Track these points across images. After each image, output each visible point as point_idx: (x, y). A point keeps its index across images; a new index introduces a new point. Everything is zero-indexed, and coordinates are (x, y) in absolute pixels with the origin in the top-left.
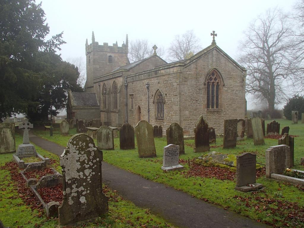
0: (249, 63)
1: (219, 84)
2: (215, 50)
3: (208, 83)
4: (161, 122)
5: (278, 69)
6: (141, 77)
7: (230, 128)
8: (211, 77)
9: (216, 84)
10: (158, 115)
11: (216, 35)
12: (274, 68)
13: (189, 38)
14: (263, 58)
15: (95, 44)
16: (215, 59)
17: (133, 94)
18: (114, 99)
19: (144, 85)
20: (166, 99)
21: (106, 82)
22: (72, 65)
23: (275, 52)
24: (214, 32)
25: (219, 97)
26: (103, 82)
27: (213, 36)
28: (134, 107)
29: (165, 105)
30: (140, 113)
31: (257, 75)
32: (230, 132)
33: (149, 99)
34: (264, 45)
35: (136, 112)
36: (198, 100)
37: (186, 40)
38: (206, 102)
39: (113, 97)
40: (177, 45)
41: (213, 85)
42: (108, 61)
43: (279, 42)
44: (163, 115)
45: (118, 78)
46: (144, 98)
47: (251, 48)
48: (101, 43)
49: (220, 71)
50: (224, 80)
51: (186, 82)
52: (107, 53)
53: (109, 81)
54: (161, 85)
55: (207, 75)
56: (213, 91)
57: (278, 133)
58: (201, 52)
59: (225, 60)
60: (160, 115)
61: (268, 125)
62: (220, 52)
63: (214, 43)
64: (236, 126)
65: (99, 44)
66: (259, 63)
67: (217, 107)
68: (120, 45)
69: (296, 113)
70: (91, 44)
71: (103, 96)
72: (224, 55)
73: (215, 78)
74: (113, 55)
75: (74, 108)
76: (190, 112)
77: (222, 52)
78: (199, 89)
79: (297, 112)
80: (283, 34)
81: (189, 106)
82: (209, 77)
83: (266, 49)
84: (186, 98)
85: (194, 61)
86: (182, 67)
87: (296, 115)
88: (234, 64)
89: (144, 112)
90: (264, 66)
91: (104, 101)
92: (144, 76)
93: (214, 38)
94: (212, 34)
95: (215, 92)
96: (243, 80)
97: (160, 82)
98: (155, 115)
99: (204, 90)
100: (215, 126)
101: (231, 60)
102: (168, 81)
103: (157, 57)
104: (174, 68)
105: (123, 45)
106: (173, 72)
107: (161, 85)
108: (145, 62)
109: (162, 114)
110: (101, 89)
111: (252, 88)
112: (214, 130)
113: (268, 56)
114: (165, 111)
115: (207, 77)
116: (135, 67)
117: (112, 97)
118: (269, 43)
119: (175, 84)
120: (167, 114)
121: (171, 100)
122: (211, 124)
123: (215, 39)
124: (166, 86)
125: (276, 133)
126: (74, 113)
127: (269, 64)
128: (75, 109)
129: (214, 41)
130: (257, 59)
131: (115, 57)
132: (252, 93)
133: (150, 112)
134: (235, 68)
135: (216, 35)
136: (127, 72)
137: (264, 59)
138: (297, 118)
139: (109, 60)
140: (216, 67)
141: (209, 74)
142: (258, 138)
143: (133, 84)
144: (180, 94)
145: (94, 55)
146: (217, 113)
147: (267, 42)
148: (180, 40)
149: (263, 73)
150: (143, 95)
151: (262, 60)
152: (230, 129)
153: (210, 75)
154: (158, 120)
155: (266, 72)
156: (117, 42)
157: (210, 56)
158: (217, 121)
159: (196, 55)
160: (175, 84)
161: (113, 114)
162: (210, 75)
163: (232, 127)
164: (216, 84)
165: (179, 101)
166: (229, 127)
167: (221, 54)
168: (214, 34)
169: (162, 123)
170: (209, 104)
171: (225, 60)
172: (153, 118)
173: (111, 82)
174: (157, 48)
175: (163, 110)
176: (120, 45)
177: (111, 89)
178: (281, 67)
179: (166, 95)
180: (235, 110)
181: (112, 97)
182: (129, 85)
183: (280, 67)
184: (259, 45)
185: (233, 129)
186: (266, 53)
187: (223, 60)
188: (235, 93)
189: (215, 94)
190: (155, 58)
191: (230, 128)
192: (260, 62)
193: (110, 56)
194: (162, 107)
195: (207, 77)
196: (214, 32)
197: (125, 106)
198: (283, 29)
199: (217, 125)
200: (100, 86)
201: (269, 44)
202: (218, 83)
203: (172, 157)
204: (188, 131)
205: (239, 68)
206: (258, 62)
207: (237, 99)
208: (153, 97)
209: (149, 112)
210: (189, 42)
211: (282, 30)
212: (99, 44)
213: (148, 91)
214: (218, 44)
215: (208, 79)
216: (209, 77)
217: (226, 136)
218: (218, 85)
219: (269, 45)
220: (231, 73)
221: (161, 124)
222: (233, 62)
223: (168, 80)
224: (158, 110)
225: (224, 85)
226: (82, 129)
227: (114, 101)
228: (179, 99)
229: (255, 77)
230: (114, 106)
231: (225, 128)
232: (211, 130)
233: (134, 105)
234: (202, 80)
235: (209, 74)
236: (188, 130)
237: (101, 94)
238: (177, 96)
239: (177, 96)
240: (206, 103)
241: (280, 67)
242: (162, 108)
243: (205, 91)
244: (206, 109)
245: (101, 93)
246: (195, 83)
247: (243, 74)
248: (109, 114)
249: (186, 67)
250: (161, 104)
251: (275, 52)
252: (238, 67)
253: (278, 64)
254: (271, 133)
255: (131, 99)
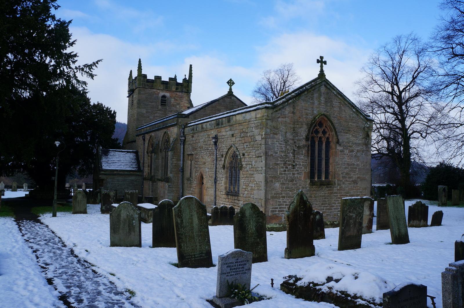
0: (373, 113)
1: (330, 140)
2: (323, 86)
3: (313, 138)
4: (235, 200)
5: (413, 123)
6: (206, 125)
7: (351, 214)
8: (317, 130)
9: (324, 140)
10: (230, 188)
11: (325, 63)
12: (407, 123)
13: (286, 76)
14: (392, 107)
15: (142, 77)
16: (324, 99)
17: (193, 153)
18: (164, 160)
19: (210, 139)
20: (243, 163)
21: (153, 134)
22: (99, 107)
23: (410, 98)
24: (322, 58)
25: (331, 161)
26: (149, 134)
27: (320, 63)
28: (193, 175)
29: (241, 172)
30: (203, 183)
31: (385, 132)
32: (351, 221)
33: (216, 162)
34: (393, 90)
35: (195, 183)
36: (296, 165)
37: (280, 78)
38: (308, 170)
39: (162, 158)
40: (265, 82)
41: (320, 142)
42: (160, 103)
43: (413, 85)
44: (238, 188)
45: (171, 128)
46: (209, 160)
47: (374, 92)
48: (151, 77)
49: (332, 119)
50: (338, 134)
51: (276, 134)
52: (159, 91)
53: (157, 132)
54: (237, 140)
55: (311, 125)
56: (321, 152)
57: (425, 222)
58: (302, 87)
59: (339, 102)
60: (234, 188)
61: (410, 207)
62: (331, 89)
63: (322, 74)
64: (361, 211)
65: (148, 78)
66: (388, 115)
67: (327, 177)
68: (180, 80)
69: (444, 189)
70: (136, 78)
71: (149, 156)
72: (338, 95)
73: (324, 130)
74: (168, 94)
75: (103, 172)
76: (283, 184)
77: (334, 90)
78: (299, 147)
79: (446, 187)
80: (419, 73)
81: (281, 174)
82: (314, 128)
83: (397, 94)
84: (277, 162)
85: (291, 101)
86: (271, 111)
87: (444, 192)
88: (354, 110)
89: (208, 182)
90: (394, 119)
91: (150, 164)
92: (210, 124)
93: (322, 67)
94: (318, 61)
95: (324, 152)
96: (368, 136)
97: (235, 135)
98: (226, 188)
99: (306, 148)
100: (324, 209)
101: (349, 103)
102: (247, 133)
103: (233, 98)
104: (257, 111)
105: (185, 80)
106: (256, 118)
107: (237, 140)
108: (214, 104)
109: (237, 187)
110: (146, 145)
111: (377, 150)
112: (321, 215)
113: (400, 104)
114: (242, 181)
115: (310, 128)
116: (198, 112)
117: (160, 158)
118: (400, 86)
119: (259, 138)
120: (244, 187)
121: (252, 165)
122: (316, 204)
123: (324, 69)
124: (243, 142)
125: (422, 221)
126: (103, 180)
127: (401, 116)
128: (105, 174)
129: (322, 71)
130: (384, 108)
131: (171, 97)
132: (376, 158)
133: (218, 182)
134: (355, 115)
135: (325, 63)
136: (185, 119)
137: (394, 108)
138: (445, 196)
139: (162, 102)
140: (326, 113)
141: (314, 122)
142: (400, 232)
143: (193, 137)
144: (266, 153)
145: (139, 93)
146: (327, 187)
147: (397, 84)
148: (271, 79)
149: (394, 128)
150: (208, 155)
151: (391, 110)
152: (351, 217)
153: (315, 126)
154: (230, 197)
155: (398, 128)
156: (176, 76)
157: (316, 95)
158: (327, 200)
159: (293, 92)
160: (259, 138)
161: (160, 184)
162: (315, 126)
163: (354, 213)
164: (324, 140)
165: (264, 165)
166: (350, 212)
167: (334, 93)
168: (321, 61)
169: (235, 201)
170: (314, 173)
171: (339, 102)
172: (221, 193)
173: (161, 133)
174: (233, 83)
175: (239, 181)
176: (180, 80)
177: (160, 145)
178: (418, 121)
179: (244, 155)
180: (355, 182)
181: (160, 158)
182: (187, 140)
183: (416, 120)
184: (386, 88)
185: (357, 215)
186: (395, 98)
187: (336, 103)
188: (355, 156)
189: (323, 156)
190: (231, 98)
191: (351, 214)
192: (388, 112)
193: (164, 97)
194: (238, 174)
195: (310, 128)
196: (322, 58)
197: (180, 173)
198: (419, 66)
199: (327, 207)
200: (144, 140)
201: (400, 87)
202: (328, 138)
203: (236, 276)
204: (278, 217)
205: (361, 117)
206: (385, 112)
207: (358, 165)
208: (223, 159)
209: (215, 183)
210: (285, 82)
211: (418, 68)
212: (148, 78)
213: (216, 150)
214: (329, 76)
215: (312, 131)
216: (314, 128)
217: (343, 228)
218: (328, 143)
219: (400, 89)
220: (350, 123)
221: (235, 204)
222: (352, 106)
223: (247, 131)
224: (230, 180)
225: (338, 142)
226: (108, 207)
227: (164, 164)
228: (264, 162)
229: (381, 135)
230: (163, 172)
231: (343, 214)
232: (317, 217)
233: (194, 171)
234: (303, 132)
235: (314, 122)
236: (278, 214)
237: (146, 153)
238: (261, 157)
239: (261, 157)
240: (309, 171)
241: (416, 120)
242: (237, 177)
243: (308, 150)
244: (308, 181)
245: (146, 151)
246: (291, 137)
247: (368, 126)
248: (155, 184)
249: (276, 111)
250: (235, 170)
251: (410, 98)
252: (359, 115)
253: (414, 116)
254: (415, 221)
255: (190, 162)
